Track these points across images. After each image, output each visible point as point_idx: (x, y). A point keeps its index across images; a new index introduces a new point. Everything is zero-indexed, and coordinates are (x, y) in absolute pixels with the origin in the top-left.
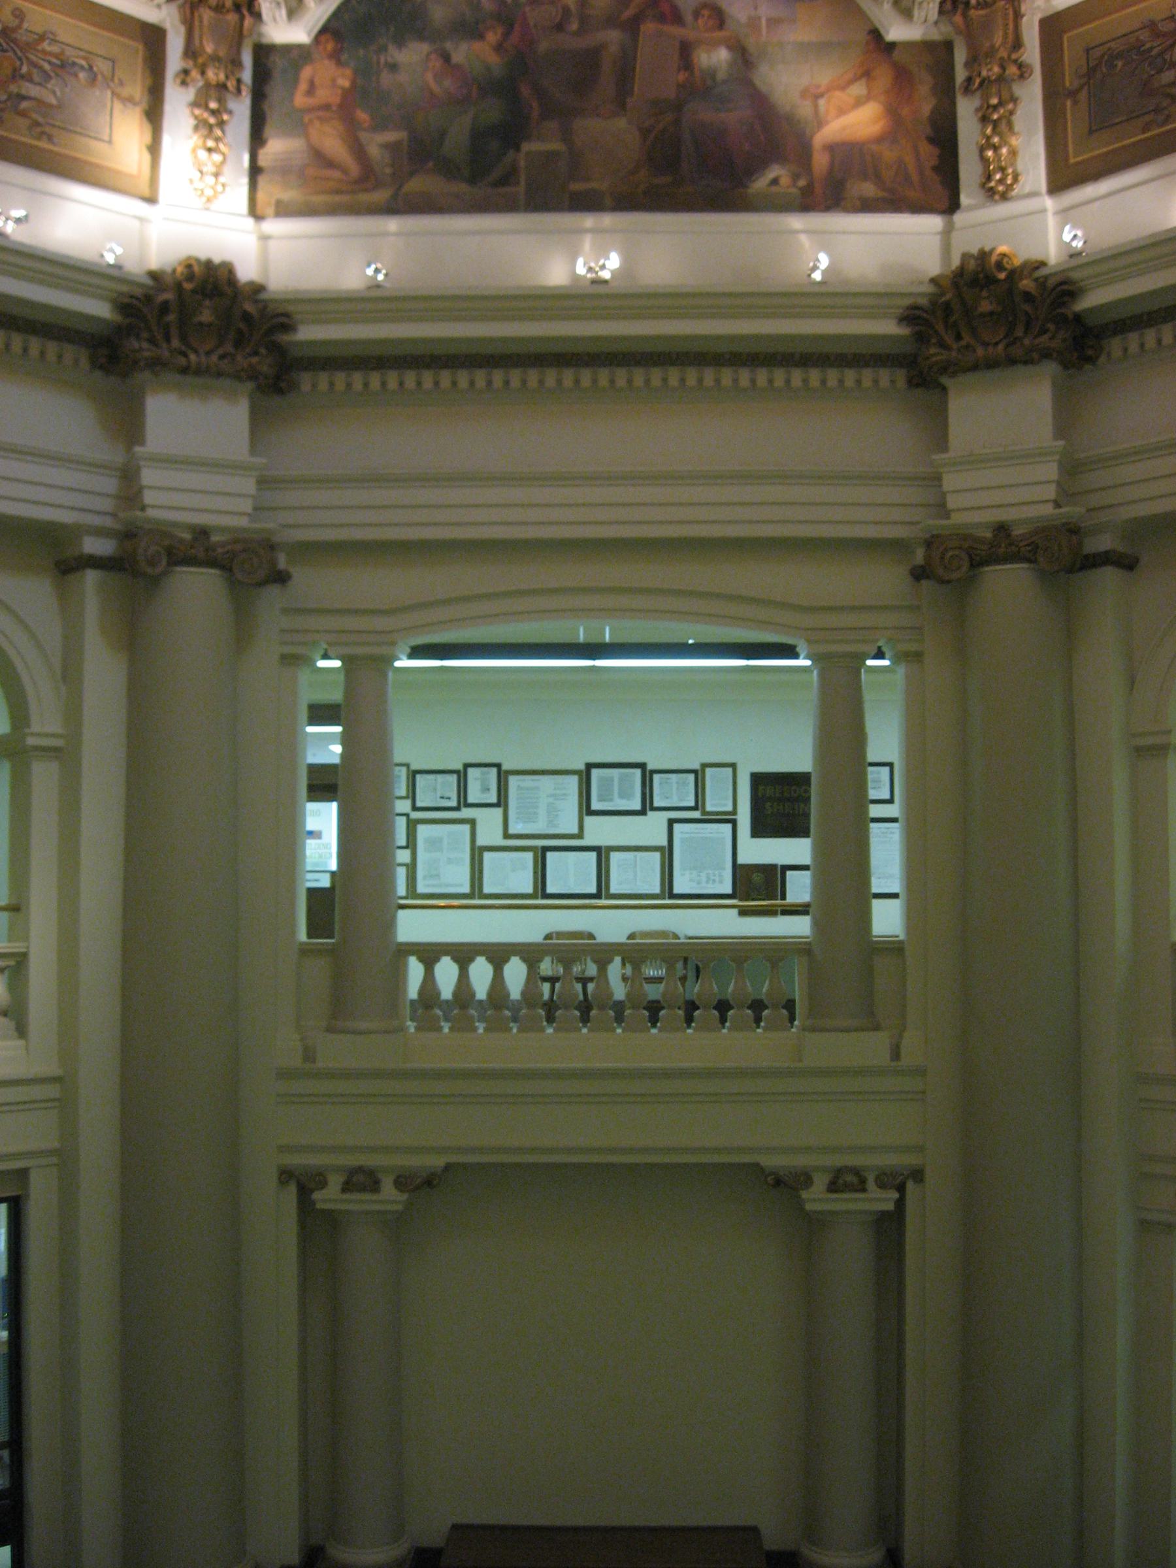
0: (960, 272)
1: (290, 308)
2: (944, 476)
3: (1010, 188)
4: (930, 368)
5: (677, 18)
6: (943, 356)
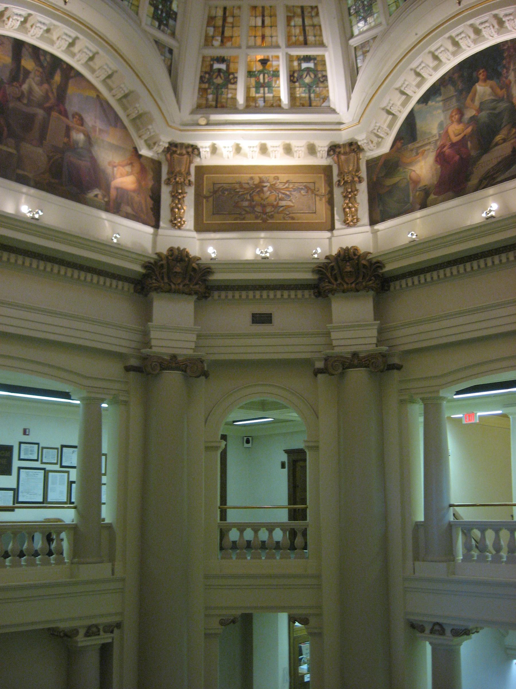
0: (339, 255)
1: (379, 259)
2: (332, 333)
3: (182, 225)
5: (65, 114)
6: (330, 287)
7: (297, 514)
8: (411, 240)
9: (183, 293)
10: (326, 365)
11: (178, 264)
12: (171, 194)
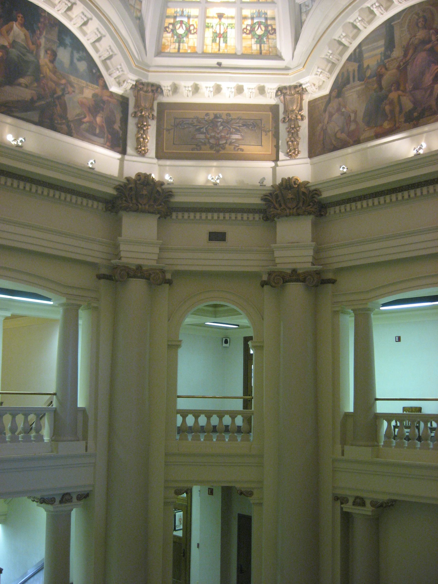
0: (281, 185)
2: (275, 252)
3: (146, 153)
4: (270, 216)
7: (247, 404)
8: (342, 172)
9: (149, 212)
10: (269, 278)
11: (145, 188)
12: (137, 125)
